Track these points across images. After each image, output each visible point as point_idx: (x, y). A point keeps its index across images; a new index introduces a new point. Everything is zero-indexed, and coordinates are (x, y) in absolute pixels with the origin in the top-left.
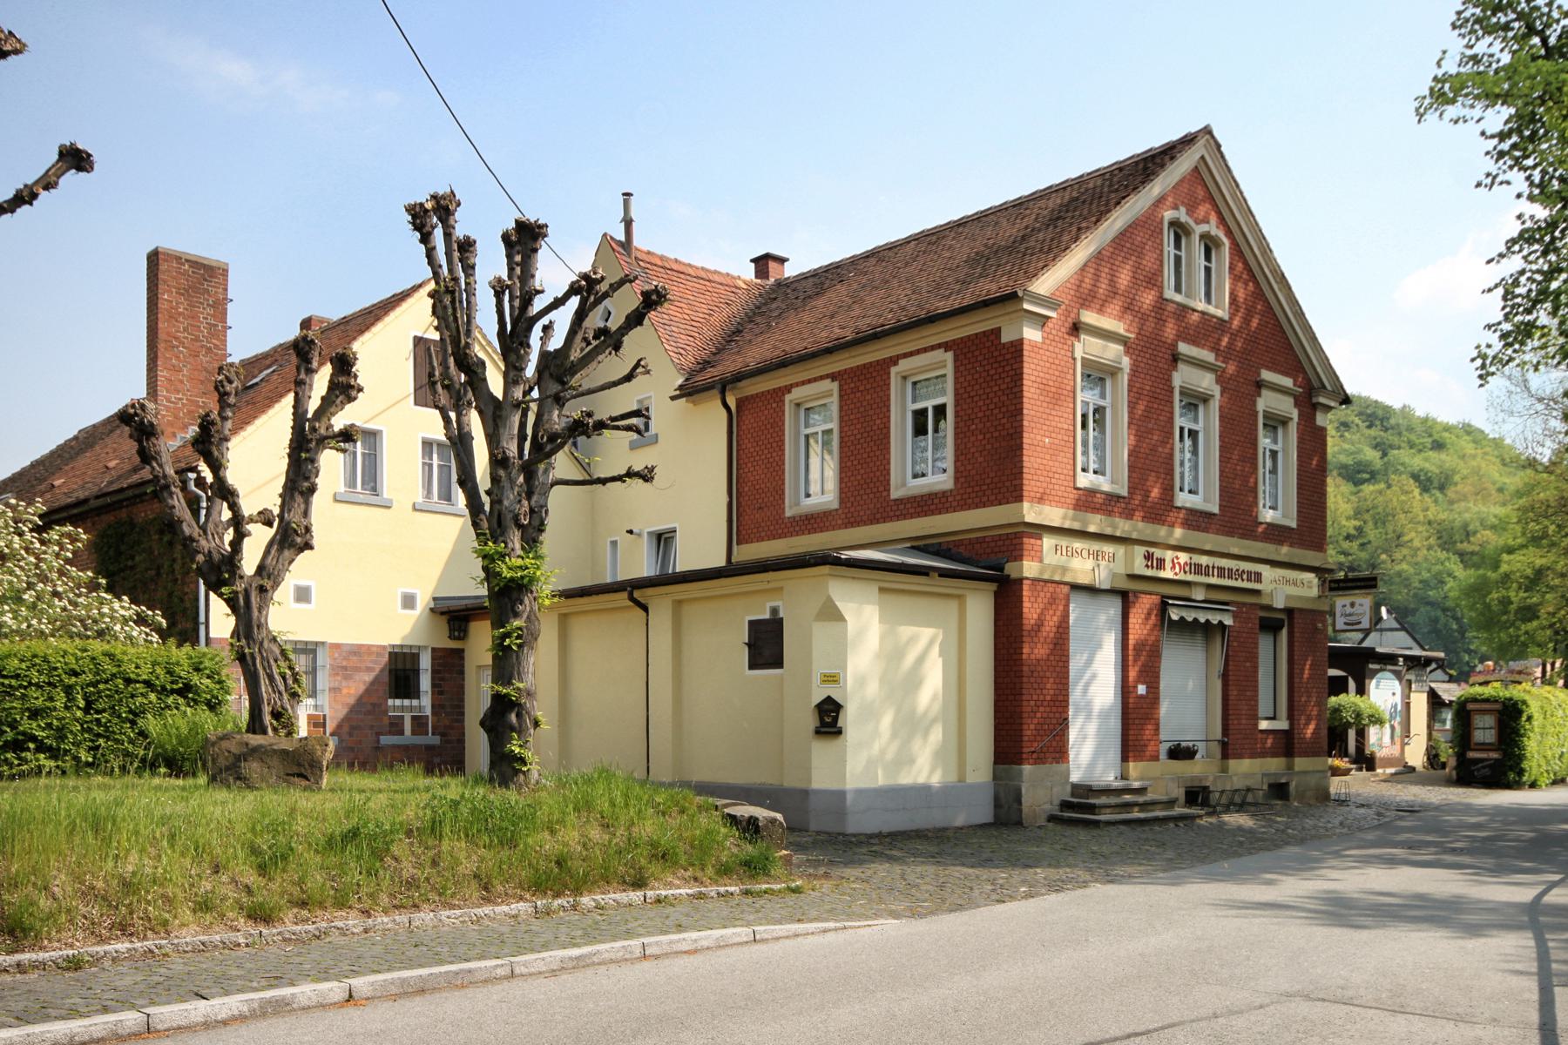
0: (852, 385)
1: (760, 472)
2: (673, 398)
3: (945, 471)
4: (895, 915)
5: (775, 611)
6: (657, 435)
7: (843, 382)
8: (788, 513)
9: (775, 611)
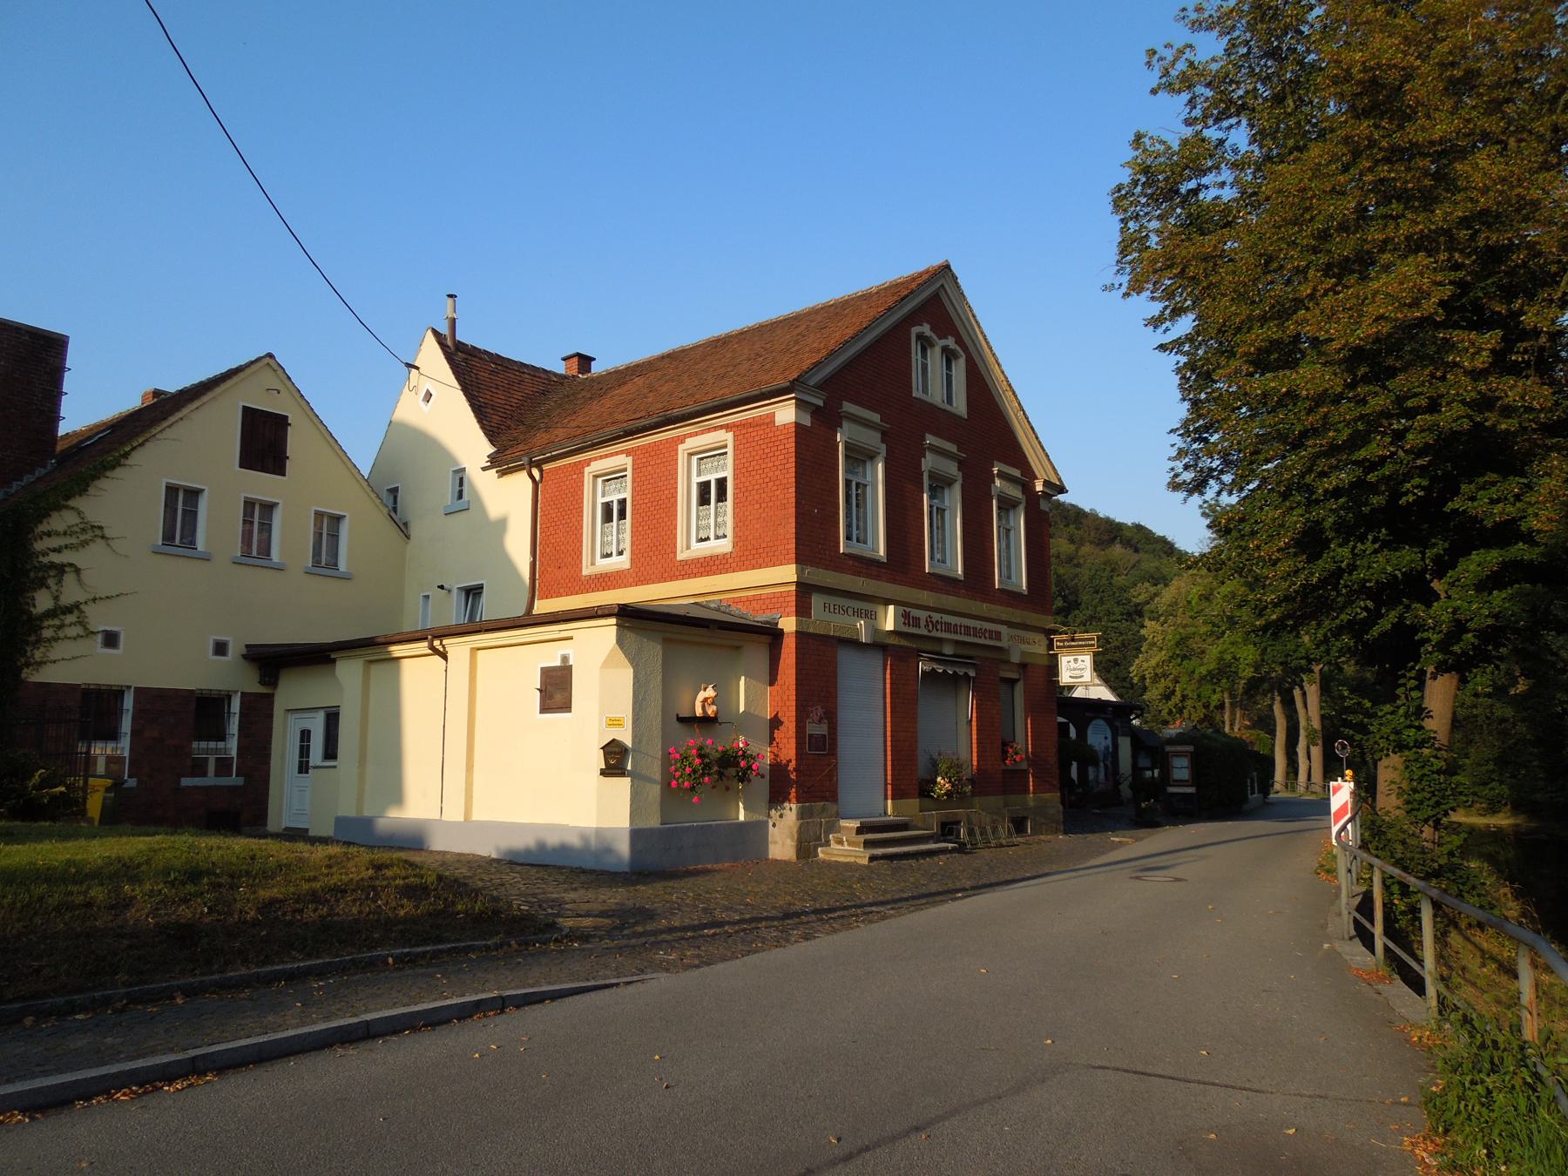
0: (645, 460)
1: (561, 535)
2: (484, 469)
3: (725, 536)
4: (667, 968)
5: (565, 658)
6: (469, 501)
7: (636, 457)
8: (585, 572)
9: (565, 658)
